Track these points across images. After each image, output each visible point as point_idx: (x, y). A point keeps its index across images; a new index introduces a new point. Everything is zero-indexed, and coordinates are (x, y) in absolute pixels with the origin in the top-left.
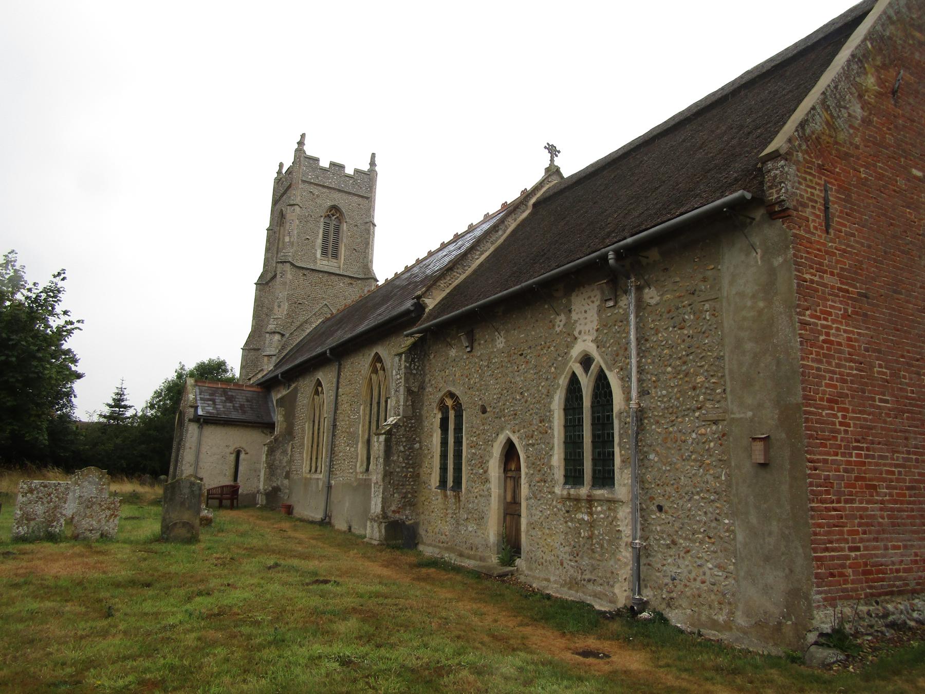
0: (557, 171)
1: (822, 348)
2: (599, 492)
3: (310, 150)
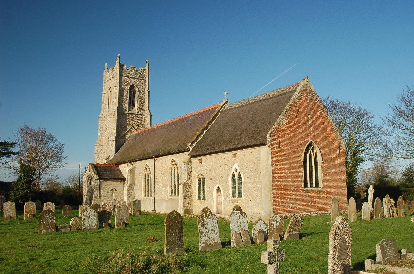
1: (277, 171)
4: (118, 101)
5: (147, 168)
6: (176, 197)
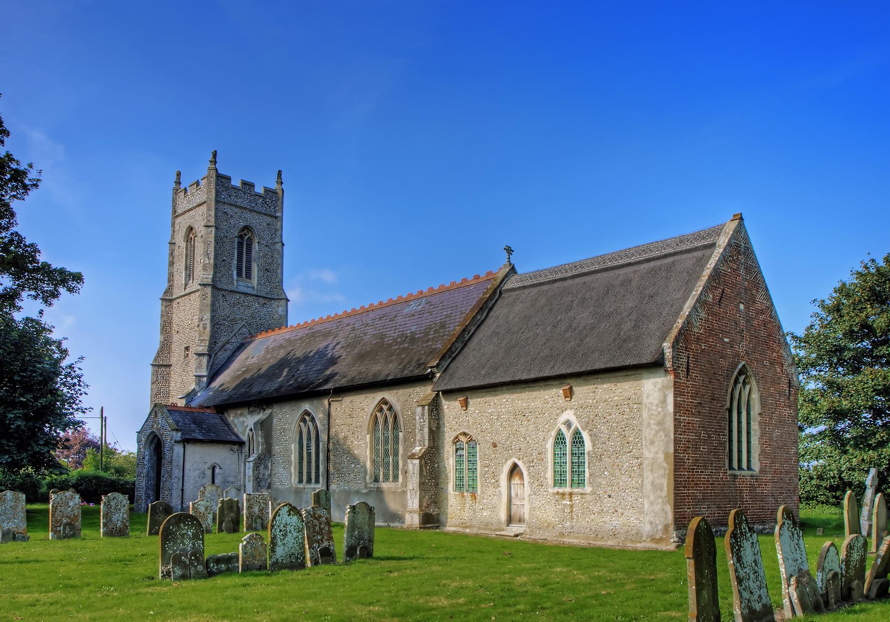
4: (212, 261)
5: (307, 418)
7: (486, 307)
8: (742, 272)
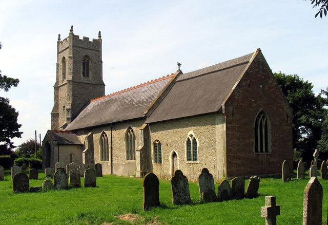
0: (181, 73)
2: (195, 162)
3: (75, 33)
6: (133, 161)
7: (168, 89)
8: (261, 72)
